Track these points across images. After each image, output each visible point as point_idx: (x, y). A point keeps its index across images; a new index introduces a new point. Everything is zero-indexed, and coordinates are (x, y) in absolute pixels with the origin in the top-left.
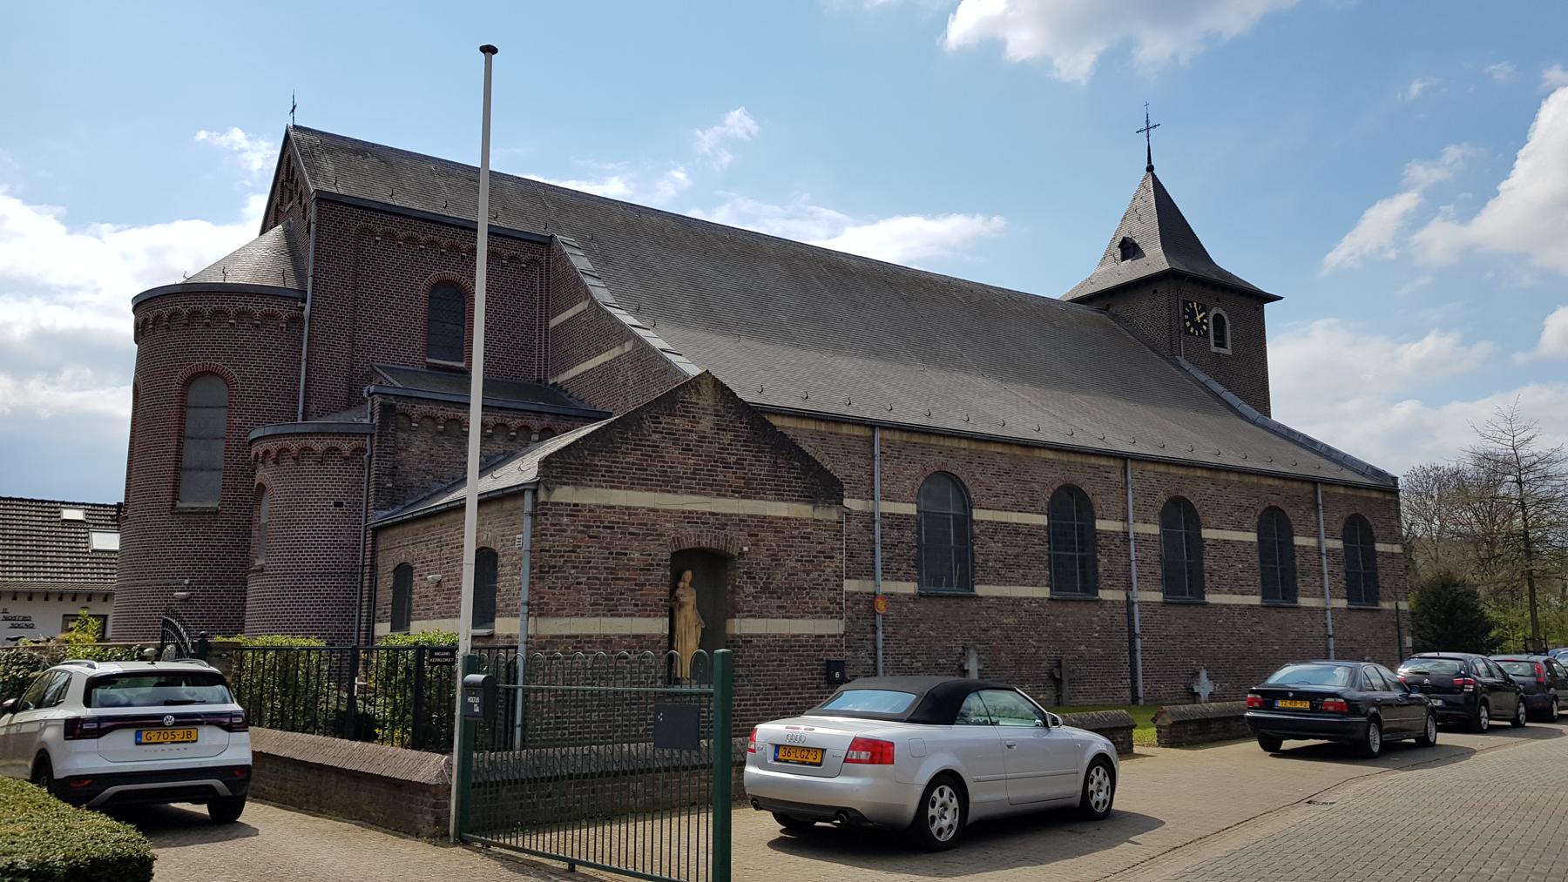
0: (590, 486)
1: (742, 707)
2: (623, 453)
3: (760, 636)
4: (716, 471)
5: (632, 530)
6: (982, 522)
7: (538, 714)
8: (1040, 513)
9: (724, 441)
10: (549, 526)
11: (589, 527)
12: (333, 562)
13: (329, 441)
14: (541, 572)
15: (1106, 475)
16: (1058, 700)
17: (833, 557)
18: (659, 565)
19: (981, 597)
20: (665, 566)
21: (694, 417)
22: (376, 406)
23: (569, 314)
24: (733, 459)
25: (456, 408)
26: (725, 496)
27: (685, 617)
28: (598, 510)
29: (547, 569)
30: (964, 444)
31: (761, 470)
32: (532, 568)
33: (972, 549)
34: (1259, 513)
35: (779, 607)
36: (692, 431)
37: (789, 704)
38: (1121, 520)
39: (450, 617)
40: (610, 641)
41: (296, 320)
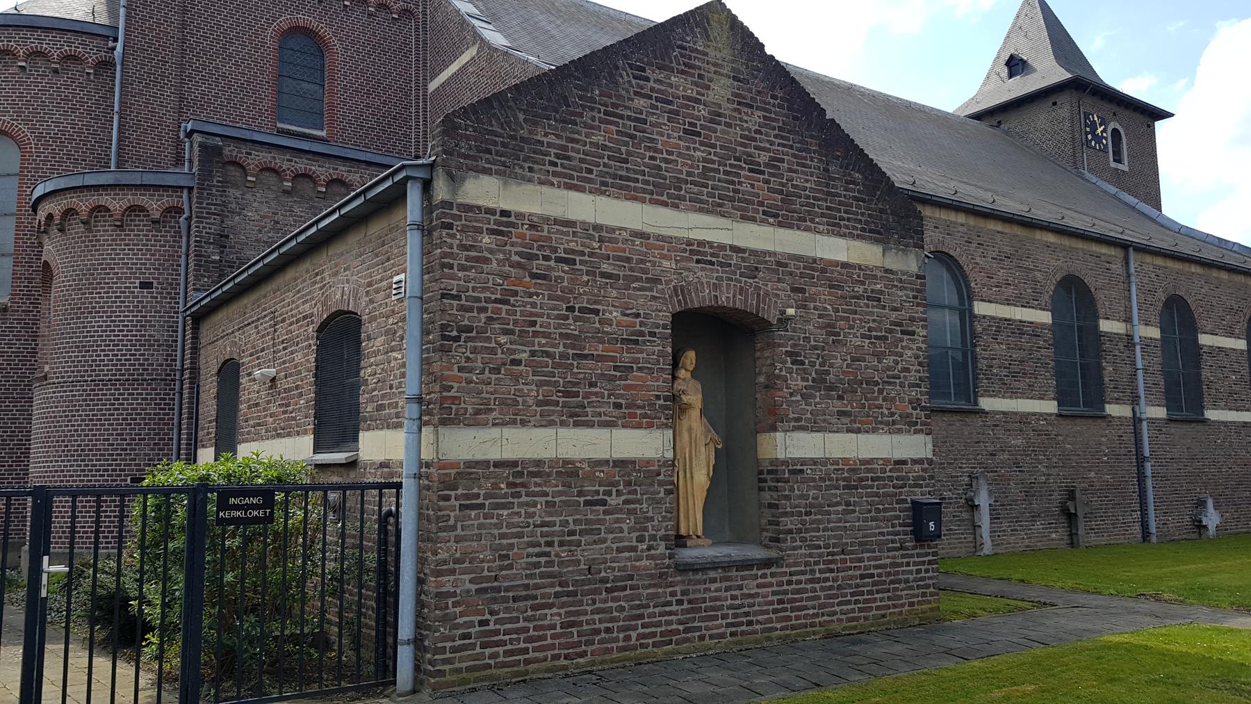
0: (530, 181)
1: (794, 586)
2: (586, 125)
3: (814, 462)
4: (738, 175)
5: (606, 267)
6: (984, 317)
7: (445, 619)
8: (1044, 310)
9: (750, 125)
10: (455, 250)
11: (530, 257)
12: (140, 365)
13: (129, 197)
14: (444, 337)
15: (1108, 265)
16: (1072, 539)
17: (913, 333)
18: (652, 334)
19: (987, 413)
20: (663, 338)
21: (701, 76)
22: (196, 146)
23: (453, 68)
24: (763, 158)
25: (307, 159)
26: (753, 220)
27: (690, 429)
28: (546, 227)
29: (454, 333)
30: (961, 218)
31: (807, 181)
32: (425, 332)
33: (973, 352)
34: (1247, 317)
35: (842, 414)
36: (698, 101)
37: (862, 577)
38: (1124, 321)
39: (289, 435)
40: (574, 473)
41: (105, 65)
